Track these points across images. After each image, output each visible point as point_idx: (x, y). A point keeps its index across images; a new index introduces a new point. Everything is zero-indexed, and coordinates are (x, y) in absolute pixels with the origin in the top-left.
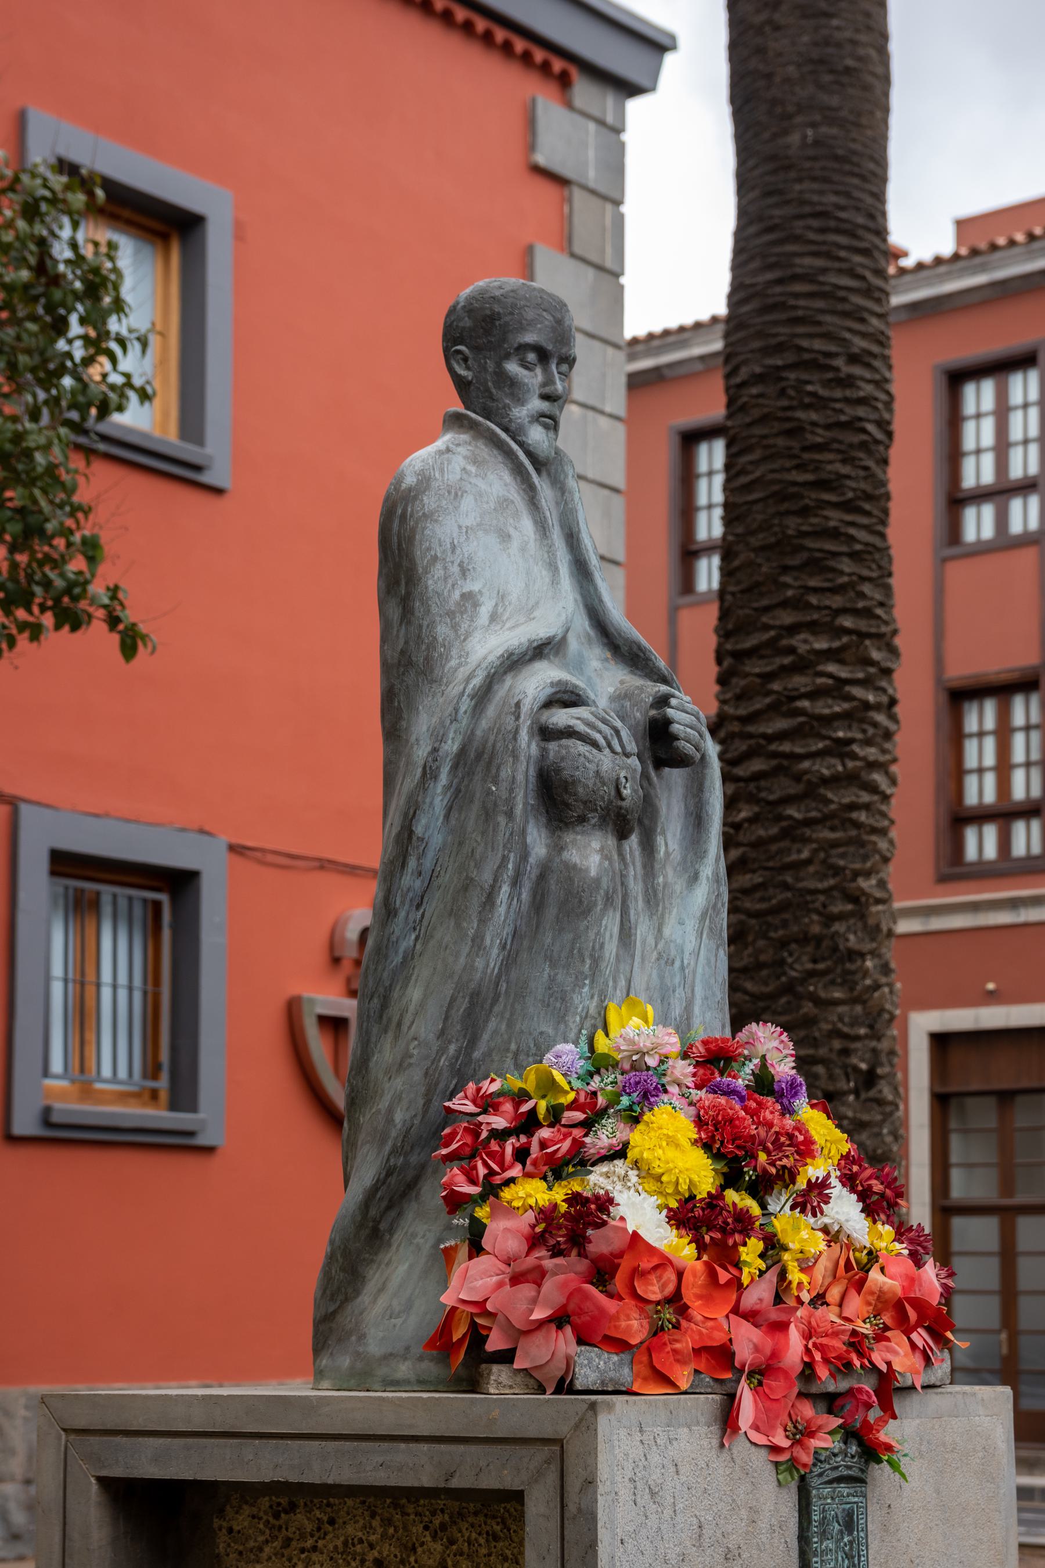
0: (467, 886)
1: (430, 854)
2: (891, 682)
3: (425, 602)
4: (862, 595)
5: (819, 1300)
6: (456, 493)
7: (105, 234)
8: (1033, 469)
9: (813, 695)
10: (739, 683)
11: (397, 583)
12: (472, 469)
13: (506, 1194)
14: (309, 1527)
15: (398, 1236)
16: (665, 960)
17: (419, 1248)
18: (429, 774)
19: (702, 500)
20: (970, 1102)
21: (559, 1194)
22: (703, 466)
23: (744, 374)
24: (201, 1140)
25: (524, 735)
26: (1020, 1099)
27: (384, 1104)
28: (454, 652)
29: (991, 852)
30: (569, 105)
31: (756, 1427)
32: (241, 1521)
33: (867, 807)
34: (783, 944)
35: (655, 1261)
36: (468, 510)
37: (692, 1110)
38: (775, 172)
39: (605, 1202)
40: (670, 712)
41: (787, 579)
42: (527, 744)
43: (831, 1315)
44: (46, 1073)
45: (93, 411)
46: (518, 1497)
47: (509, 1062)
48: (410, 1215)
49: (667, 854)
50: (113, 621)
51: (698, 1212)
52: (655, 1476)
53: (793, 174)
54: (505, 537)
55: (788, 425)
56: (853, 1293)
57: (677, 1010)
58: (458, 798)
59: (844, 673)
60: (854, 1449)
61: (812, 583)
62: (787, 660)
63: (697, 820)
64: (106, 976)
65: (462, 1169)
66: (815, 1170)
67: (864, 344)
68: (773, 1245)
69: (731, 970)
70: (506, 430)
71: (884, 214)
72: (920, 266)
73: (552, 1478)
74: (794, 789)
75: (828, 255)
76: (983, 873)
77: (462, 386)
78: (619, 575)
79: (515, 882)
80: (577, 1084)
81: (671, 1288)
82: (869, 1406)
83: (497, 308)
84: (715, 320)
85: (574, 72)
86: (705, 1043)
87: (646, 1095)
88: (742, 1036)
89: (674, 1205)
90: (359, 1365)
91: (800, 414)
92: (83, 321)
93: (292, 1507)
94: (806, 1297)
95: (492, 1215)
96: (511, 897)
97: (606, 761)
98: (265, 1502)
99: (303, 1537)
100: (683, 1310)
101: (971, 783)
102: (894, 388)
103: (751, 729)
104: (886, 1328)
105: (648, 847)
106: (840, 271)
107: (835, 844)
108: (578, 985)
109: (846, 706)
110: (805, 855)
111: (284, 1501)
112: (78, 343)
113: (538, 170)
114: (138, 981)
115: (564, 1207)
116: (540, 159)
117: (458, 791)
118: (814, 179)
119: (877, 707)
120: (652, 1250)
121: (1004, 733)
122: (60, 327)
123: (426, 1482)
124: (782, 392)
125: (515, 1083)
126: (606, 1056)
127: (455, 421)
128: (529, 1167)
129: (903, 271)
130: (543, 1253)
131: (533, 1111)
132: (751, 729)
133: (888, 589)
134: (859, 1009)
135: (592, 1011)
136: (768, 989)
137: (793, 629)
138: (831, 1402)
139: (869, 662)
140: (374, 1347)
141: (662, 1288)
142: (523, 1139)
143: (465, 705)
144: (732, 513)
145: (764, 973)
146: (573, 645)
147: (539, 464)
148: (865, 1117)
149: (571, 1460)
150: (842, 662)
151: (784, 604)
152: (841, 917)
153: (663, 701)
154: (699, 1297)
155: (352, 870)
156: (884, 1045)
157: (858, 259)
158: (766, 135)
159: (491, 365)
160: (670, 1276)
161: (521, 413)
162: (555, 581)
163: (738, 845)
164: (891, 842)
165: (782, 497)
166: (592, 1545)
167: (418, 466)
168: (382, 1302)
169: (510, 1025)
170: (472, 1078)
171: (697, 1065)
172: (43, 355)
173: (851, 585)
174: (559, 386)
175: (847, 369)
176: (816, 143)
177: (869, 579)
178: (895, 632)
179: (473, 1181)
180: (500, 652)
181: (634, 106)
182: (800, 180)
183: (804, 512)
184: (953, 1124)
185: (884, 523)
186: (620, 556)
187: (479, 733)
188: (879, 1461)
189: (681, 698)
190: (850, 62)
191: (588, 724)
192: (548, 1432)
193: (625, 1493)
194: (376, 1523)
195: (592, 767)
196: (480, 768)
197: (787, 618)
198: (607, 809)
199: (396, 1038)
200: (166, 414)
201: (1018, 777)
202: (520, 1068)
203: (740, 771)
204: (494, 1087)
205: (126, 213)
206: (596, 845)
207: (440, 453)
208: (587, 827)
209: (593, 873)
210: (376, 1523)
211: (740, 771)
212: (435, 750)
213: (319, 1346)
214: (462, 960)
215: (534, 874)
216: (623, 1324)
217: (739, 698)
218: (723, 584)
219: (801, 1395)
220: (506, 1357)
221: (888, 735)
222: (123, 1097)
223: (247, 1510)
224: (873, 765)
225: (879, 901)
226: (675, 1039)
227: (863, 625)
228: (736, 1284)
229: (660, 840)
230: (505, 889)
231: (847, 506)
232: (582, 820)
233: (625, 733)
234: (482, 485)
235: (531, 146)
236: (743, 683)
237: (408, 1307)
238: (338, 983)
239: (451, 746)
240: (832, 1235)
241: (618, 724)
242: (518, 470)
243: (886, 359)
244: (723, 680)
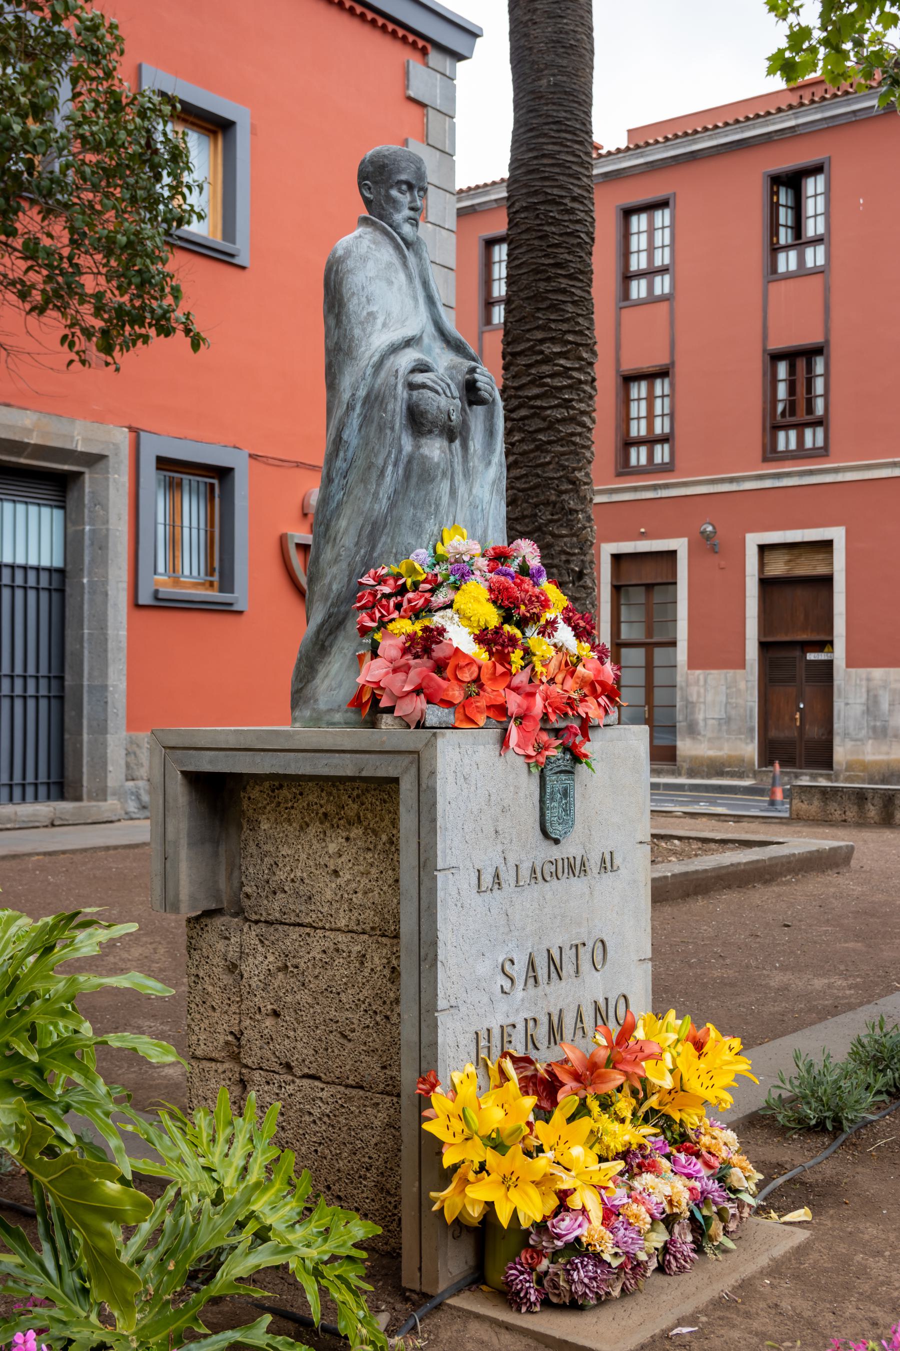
0: (370, 466)
1: (351, 450)
2: (592, 369)
3: (348, 317)
4: (578, 324)
5: (552, 681)
6: (364, 259)
7: (180, 129)
8: (667, 261)
9: (552, 376)
10: (514, 369)
11: (334, 306)
12: (373, 246)
13: (390, 627)
14: (290, 796)
15: (334, 649)
16: (474, 506)
17: (345, 655)
18: (350, 407)
19: (496, 275)
20: (630, 589)
21: (417, 627)
22: (496, 258)
23: (517, 206)
24: (235, 608)
25: (400, 387)
26: (656, 588)
27: (327, 581)
28: (363, 343)
29: (643, 461)
30: (427, 65)
31: (518, 746)
32: (255, 794)
33: (580, 434)
34: (536, 506)
35: (467, 662)
36: (371, 269)
37: (487, 584)
38: (534, 99)
39: (441, 631)
40: (476, 376)
41: (540, 315)
42: (402, 392)
43: (558, 689)
44: (155, 573)
45: (175, 224)
46: (396, 781)
47: (392, 558)
48: (340, 638)
49: (475, 451)
50: (187, 331)
51: (489, 636)
52: (466, 770)
53: (543, 101)
54: (390, 283)
55: (540, 234)
56: (569, 677)
57: (479, 532)
58: (366, 420)
59: (568, 364)
60: (568, 756)
61: (552, 317)
62: (539, 357)
63: (490, 433)
64: (186, 522)
65: (368, 614)
66: (549, 615)
67: (579, 191)
68: (528, 653)
69: (508, 519)
70: (391, 226)
71: (590, 123)
72: (609, 153)
73: (413, 770)
74: (543, 425)
75: (561, 144)
76: (640, 471)
77: (368, 202)
78: (453, 313)
79: (395, 465)
80: (427, 570)
81: (475, 675)
82: (576, 735)
83: (386, 161)
84: (503, 180)
85: (429, 47)
86: (494, 549)
87: (463, 576)
88: (513, 546)
89: (477, 632)
90: (315, 715)
91: (546, 228)
92: (169, 174)
93: (281, 787)
94: (545, 680)
95: (383, 638)
96: (393, 472)
97: (443, 401)
98: (267, 784)
99: (286, 801)
100: (481, 686)
101: (634, 425)
102: (595, 215)
103: (520, 393)
104: (586, 696)
105: (465, 447)
106: (567, 152)
107: (563, 454)
108: (428, 518)
109: (569, 381)
110: (548, 459)
111: (277, 784)
112: (166, 188)
113: (411, 99)
114: (202, 525)
115: (420, 633)
116: (411, 93)
117: (365, 416)
118: (554, 104)
119: (586, 382)
120: (465, 656)
121: (651, 399)
122: (158, 178)
123: (349, 773)
124: (537, 217)
125: (395, 569)
126: (442, 556)
127: (365, 221)
128: (402, 613)
129: (600, 156)
130: (409, 657)
131: (404, 584)
132: (520, 393)
133: (591, 321)
134: (575, 539)
135: (435, 532)
136: (527, 529)
137: (542, 341)
138: (557, 732)
139: (581, 359)
140: (322, 706)
141: (471, 674)
142: (399, 598)
143: (369, 371)
144: (511, 280)
145: (527, 520)
146: (426, 340)
147: (408, 244)
148: (578, 595)
149: (423, 762)
150: (567, 359)
151: (538, 328)
152: (566, 492)
153: (473, 370)
154: (490, 679)
155: (313, 468)
156: (588, 558)
157: (577, 146)
158: (529, 80)
159: (383, 191)
160: (475, 669)
161: (399, 217)
162: (416, 306)
163: (514, 454)
164: (592, 453)
165: (536, 271)
166: (434, 804)
167: (345, 245)
168: (326, 682)
169: (393, 539)
170: (373, 567)
171: (490, 560)
172: (149, 191)
173: (573, 318)
174: (419, 203)
175: (571, 205)
176: (555, 84)
177: (582, 315)
178: (595, 343)
179: (373, 620)
180: (387, 343)
181: (460, 65)
182: (547, 104)
183: (548, 279)
184: (622, 601)
185: (590, 286)
186: (453, 305)
187: (376, 386)
188: (581, 763)
189: (482, 369)
190: (572, 42)
191: (434, 382)
192: (411, 748)
193: (451, 779)
194: (324, 794)
195: (435, 404)
196: (377, 405)
197: (539, 335)
198: (443, 427)
199: (333, 546)
200: (215, 227)
201: (658, 422)
202: (397, 562)
203: (514, 415)
204: (384, 572)
205: (191, 119)
206: (437, 445)
207: (356, 238)
208: (433, 436)
209: (436, 460)
210: (324, 794)
211: (514, 415)
212: (353, 395)
213: (295, 705)
214: (368, 505)
215: (406, 460)
216: (451, 693)
217: (514, 377)
218: (506, 318)
219: (541, 729)
220: (390, 710)
221: (591, 397)
222: (195, 585)
223: (257, 788)
224: (583, 413)
225: (585, 484)
226: (478, 547)
227: (578, 339)
228: (508, 673)
229: (471, 443)
230: (390, 468)
231: (570, 277)
232: (430, 432)
233: (453, 386)
234: (378, 255)
235: (407, 87)
236: (516, 369)
237: (340, 685)
238: (306, 527)
239: (362, 393)
240: (558, 648)
241: (449, 382)
242: (397, 247)
243: (591, 199)
244: (506, 368)
